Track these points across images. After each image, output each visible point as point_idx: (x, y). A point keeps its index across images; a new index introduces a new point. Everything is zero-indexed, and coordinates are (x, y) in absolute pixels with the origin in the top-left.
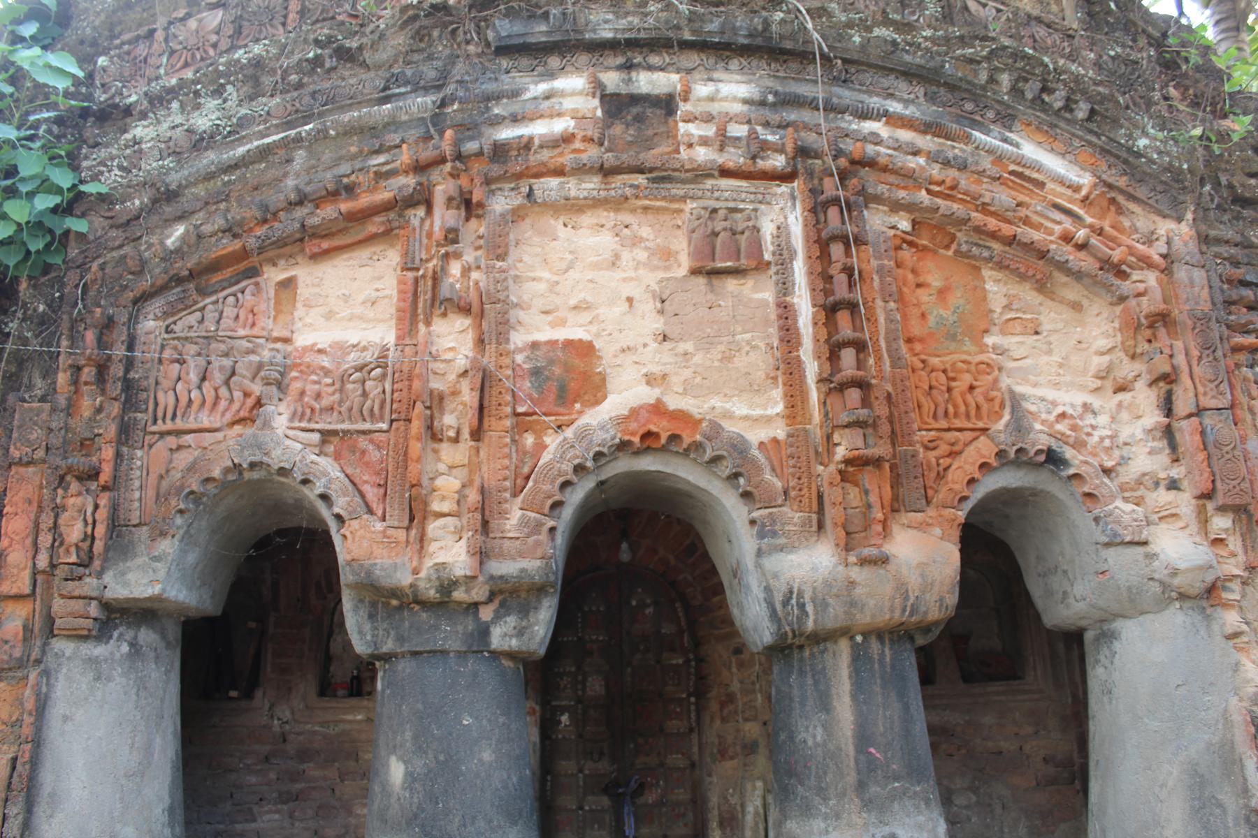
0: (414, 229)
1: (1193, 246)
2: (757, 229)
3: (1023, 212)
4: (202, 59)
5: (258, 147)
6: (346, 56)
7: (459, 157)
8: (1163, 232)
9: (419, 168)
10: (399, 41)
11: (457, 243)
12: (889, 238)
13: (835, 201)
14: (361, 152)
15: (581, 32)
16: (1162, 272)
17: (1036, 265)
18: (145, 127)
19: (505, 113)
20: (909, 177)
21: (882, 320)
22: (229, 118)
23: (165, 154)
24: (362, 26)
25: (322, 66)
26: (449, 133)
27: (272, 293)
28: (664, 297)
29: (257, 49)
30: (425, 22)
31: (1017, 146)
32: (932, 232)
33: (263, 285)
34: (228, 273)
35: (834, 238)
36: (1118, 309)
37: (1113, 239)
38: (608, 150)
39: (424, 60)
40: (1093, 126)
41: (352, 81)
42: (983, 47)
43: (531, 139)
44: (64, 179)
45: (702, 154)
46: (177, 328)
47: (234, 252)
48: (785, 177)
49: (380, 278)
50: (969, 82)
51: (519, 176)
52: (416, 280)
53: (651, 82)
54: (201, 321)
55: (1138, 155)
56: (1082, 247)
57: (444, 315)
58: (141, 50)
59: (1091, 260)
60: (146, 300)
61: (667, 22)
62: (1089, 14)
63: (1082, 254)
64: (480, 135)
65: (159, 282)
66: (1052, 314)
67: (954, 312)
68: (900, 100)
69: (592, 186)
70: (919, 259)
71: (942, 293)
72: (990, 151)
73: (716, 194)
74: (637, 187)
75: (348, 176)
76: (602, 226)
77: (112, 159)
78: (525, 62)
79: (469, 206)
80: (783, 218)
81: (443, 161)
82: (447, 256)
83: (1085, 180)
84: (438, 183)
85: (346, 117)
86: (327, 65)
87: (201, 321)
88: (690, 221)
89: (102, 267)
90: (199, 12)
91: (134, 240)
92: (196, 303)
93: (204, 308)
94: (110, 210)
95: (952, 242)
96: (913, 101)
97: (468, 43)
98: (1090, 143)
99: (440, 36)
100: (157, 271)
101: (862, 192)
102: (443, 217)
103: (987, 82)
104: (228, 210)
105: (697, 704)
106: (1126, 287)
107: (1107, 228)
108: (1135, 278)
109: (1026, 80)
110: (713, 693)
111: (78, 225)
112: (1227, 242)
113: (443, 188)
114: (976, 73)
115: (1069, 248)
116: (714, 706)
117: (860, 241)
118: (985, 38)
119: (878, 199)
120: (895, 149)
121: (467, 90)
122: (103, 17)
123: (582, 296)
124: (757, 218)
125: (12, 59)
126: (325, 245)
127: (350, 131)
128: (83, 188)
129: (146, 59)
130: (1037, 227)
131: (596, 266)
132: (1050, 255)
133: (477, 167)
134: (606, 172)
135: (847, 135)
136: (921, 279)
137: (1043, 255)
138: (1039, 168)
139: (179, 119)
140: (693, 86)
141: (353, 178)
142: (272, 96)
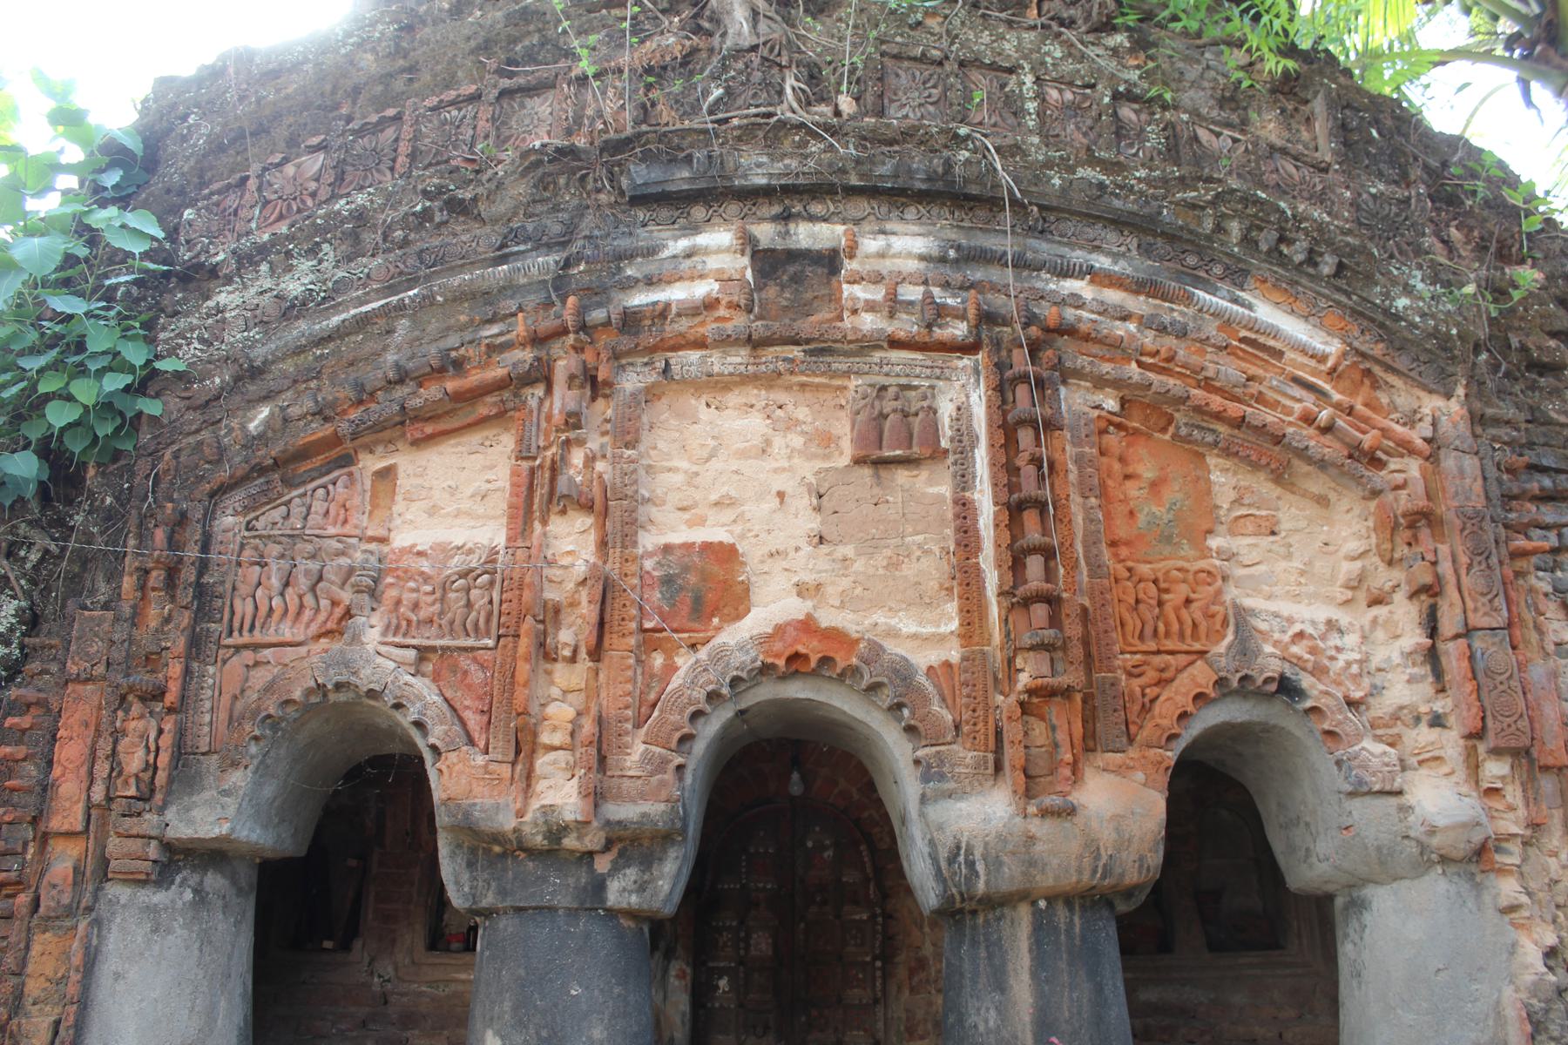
1: (1464, 428)
3: (1254, 388)
4: (299, 211)
6: (458, 208)
7: (583, 327)
9: (538, 340)
10: (520, 190)
12: (1092, 420)
13: (1024, 378)
14: (472, 321)
16: (1427, 459)
17: (1272, 454)
18: (230, 293)
19: (639, 275)
20: (1117, 349)
21: (1079, 519)
24: (477, 172)
25: (431, 220)
26: (571, 300)
29: (360, 199)
30: (549, 168)
31: (1250, 307)
32: (1144, 412)
33: (357, 475)
34: (318, 461)
35: (1021, 422)
36: (1373, 505)
37: (1366, 420)
38: (760, 317)
40: (1342, 283)
41: (464, 238)
42: (1207, 190)
43: (668, 305)
44: (136, 355)
46: (259, 525)
49: (492, 467)
50: (1191, 232)
51: (653, 350)
52: (532, 471)
53: (812, 236)
55: (1397, 317)
56: (1328, 429)
57: (563, 512)
58: (232, 201)
59: (1337, 445)
61: (830, 165)
63: (1327, 439)
65: (239, 473)
66: (1293, 510)
68: (1109, 254)
69: (739, 360)
70: (1129, 445)
71: (1155, 486)
72: (1216, 315)
73: (886, 369)
74: (792, 361)
77: (192, 330)
78: (665, 213)
79: (593, 384)
80: (963, 397)
84: (560, 358)
85: (455, 281)
86: (437, 219)
88: (854, 399)
89: (176, 456)
90: (298, 156)
91: (213, 424)
92: (281, 495)
93: (290, 501)
94: (187, 389)
95: (1170, 423)
96: (1123, 255)
97: (599, 191)
98: (1338, 303)
99: (567, 184)
101: (1058, 365)
102: (563, 399)
103: (1213, 231)
105: (883, 969)
106: (1380, 478)
107: (1359, 407)
108: (1392, 466)
109: (1261, 229)
110: (901, 957)
111: (152, 407)
112: (1508, 422)
113: (564, 364)
114: (1200, 224)
115: (1311, 431)
116: (902, 973)
117: (1052, 425)
118: (1209, 180)
119: (1078, 374)
120: (1100, 314)
121: (597, 247)
123: (724, 490)
124: (934, 396)
126: (429, 429)
127: (460, 297)
128: (158, 365)
129: (236, 213)
130: (1274, 405)
131: (743, 454)
132: (1286, 440)
133: (604, 339)
134: (756, 344)
136: (1130, 470)
137: (1278, 440)
138: (1275, 333)
140: (860, 240)
141: (462, 351)
142: (373, 255)
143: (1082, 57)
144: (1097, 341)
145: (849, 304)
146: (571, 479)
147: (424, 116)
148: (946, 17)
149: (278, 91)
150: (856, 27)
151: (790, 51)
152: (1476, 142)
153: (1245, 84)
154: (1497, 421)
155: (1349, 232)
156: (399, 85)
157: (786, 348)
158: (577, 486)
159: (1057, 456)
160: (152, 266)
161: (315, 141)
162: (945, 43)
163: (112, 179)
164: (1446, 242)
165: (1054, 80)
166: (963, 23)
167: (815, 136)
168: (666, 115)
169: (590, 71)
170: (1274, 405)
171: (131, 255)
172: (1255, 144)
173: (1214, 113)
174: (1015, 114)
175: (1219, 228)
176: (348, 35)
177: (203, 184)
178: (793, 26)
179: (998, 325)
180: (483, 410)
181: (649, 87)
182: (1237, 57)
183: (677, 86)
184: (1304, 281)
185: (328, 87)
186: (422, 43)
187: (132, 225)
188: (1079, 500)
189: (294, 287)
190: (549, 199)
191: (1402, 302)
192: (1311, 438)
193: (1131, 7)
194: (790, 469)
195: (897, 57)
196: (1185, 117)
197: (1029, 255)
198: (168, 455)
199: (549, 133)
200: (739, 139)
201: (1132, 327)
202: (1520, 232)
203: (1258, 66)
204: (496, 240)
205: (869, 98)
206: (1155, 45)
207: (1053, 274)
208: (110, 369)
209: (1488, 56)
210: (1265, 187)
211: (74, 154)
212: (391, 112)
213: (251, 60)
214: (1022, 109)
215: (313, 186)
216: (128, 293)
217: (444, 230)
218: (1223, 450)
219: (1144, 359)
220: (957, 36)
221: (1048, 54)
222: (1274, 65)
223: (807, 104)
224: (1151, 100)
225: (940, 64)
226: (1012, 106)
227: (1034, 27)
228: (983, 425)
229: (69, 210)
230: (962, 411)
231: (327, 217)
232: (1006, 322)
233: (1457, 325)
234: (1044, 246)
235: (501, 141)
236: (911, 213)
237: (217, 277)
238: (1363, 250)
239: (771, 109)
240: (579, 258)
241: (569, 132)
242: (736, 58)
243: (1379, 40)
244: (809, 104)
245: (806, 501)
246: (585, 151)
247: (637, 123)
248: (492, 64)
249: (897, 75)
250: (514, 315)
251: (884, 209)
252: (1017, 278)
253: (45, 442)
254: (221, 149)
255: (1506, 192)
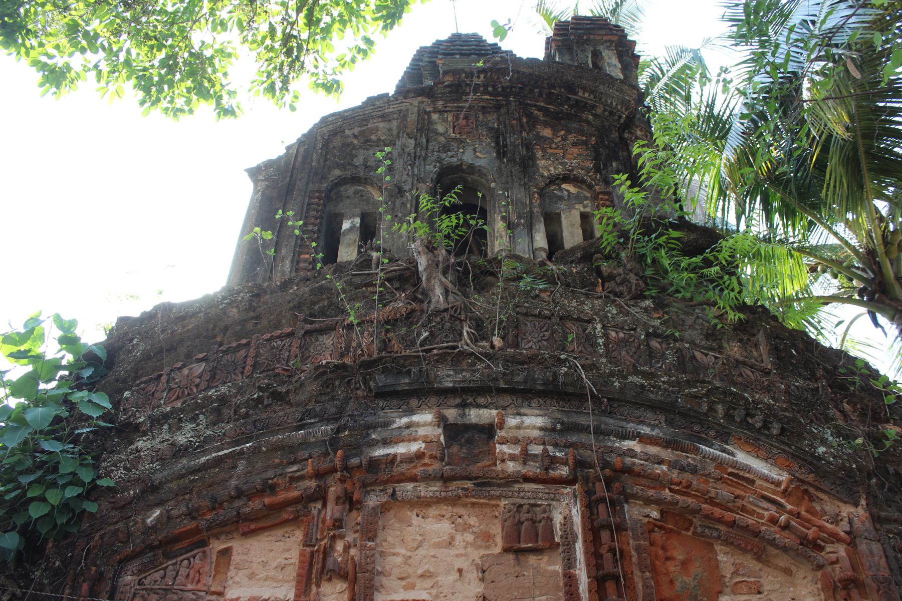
0: (313, 517)
1: (868, 524)
2: (550, 519)
3: (740, 503)
4: (189, 395)
5: (214, 458)
6: (278, 397)
7: (346, 468)
8: (845, 515)
9: (319, 475)
10: (313, 388)
11: (342, 528)
12: (644, 524)
13: (603, 500)
14: (282, 462)
15: (432, 384)
16: (849, 544)
17: (753, 543)
18: (144, 441)
19: (378, 438)
20: (657, 481)
21: (640, 586)
22: (199, 437)
23: (155, 460)
24: (290, 376)
25: (262, 403)
26: (340, 452)
27: (214, 557)
28: (485, 568)
29: (223, 389)
30: (330, 376)
31: (733, 454)
32: (675, 519)
33: (208, 553)
34: (185, 543)
35: (603, 527)
36: (819, 574)
37: (808, 521)
38: (447, 464)
39: (328, 401)
40: (785, 439)
41: (280, 414)
42: (703, 388)
43: (395, 456)
44: (86, 476)
45: (511, 467)
46: (146, 582)
47: (191, 529)
48: (568, 482)
49: (288, 550)
50: (695, 411)
51: (386, 482)
52: (312, 553)
53: (479, 416)
54: (164, 577)
55: (819, 458)
56: (786, 527)
57: (330, 580)
58: (152, 388)
59: (792, 537)
60: (128, 561)
61: (489, 376)
62: (778, 358)
63: (786, 533)
64: (361, 453)
65: (138, 549)
66: (770, 577)
67: (695, 578)
68: (648, 425)
69: (436, 489)
70: (667, 539)
71: (685, 564)
72: (714, 459)
73: (522, 494)
74: (466, 489)
75: (272, 479)
76: (443, 516)
77: (121, 462)
78: (395, 402)
79: (351, 502)
80: (568, 512)
81: (335, 471)
82: (334, 538)
83: (784, 477)
84: (331, 486)
85: (274, 439)
86: (265, 403)
87: (164, 577)
88: (503, 513)
89: (102, 537)
90: (191, 363)
91: (127, 518)
92: (161, 564)
93: (166, 567)
94: (113, 497)
95: (691, 525)
96: (657, 425)
97: (357, 389)
98: (784, 451)
99: (340, 385)
100: (138, 541)
101: (623, 492)
102: (332, 511)
103: (708, 411)
104: (190, 500)
106: (822, 557)
107: (803, 513)
108: (828, 550)
109: (735, 409)
111: (91, 507)
112: (895, 521)
113: (334, 490)
114: (700, 406)
115: (776, 528)
117: (621, 528)
118: (703, 382)
119: (635, 496)
120: (645, 460)
121: (355, 421)
122: (132, 365)
123: (427, 567)
124: (550, 511)
125: (69, 398)
126: (253, 526)
127: (275, 448)
128: (99, 482)
129: (153, 394)
130: (752, 513)
131: (438, 545)
132: (762, 534)
133: (357, 476)
134: (446, 479)
135: (612, 451)
136: (669, 554)
137: (757, 534)
138: (749, 469)
139: (167, 436)
140: (506, 419)
141: (275, 480)
142: (228, 422)
143: (628, 314)
144: (645, 477)
145: (500, 456)
146: (335, 560)
147: (262, 344)
148: (552, 292)
149: (183, 327)
150: (502, 298)
151: (466, 312)
152: (853, 353)
153: (719, 326)
154: (888, 520)
155: (786, 410)
156: (250, 326)
157: (463, 482)
158: (339, 564)
159: (624, 547)
160: (103, 424)
161: (201, 356)
162: (551, 306)
163: (87, 373)
164: (842, 412)
165: (613, 327)
166: (561, 296)
167: (480, 360)
168: (396, 346)
169: (355, 322)
170: (752, 513)
171: (92, 418)
172: (727, 360)
173: (703, 343)
174: (592, 345)
175: (711, 409)
176: (224, 298)
177: (137, 377)
178: (468, 297)
179: (587, 468)
180: (285, 516)
181: (387, 331)
182: (712, 312)
183: (403, 330)
184: (762, 438)
185: (211, 326)
186: (264, 303)
187: (94, 401)
188: (639, 574)
189: (181, 439)
190: (329, 393)
191: (821, 449)
192: (776, 533)
193: (653, 286)
194: (466, 555)
195: (526, 315)
196: (687, 345)
197: (603, 427)
198: (97, 537)
199: (331, 355)
200: (437, 361)
201: (665, 468)
202: (884, 405)
203: (725, 316)
204: (298, 416)
205: (510, 338)
206: (667, 306)
207: (617, 438)
208: (70, 483)
209: (850, 300)
210: (735, 384)
211: (69, 358)
212: (244, 341)
213: (171, 310)
214: (596, 343)
215: (198, 380)
216: (87, 438)
217: (269, 409)
218: (724, 541)
219: (673, 487)
220: (558, 303)
221: (609, 312)
222: (733, 316)
223: (475, 341)
224: (667, 336)
225: (550, 318)
226: (589, 341)
227: (601, 297)
228: (580, 528)
229: (60, 392)
230: (567, 519)
231: (204, 398)
232: (591, 466)
233: (856, 462)
234: (612, 421)
235: (304, 359)
236: (535, 403)
237: (139, 431)
238: (795, 420)
239: (455, 344)
240: (345, 427)
241: (342, 355)
242: (436, 315)
243: (790, 291)
244: (476, 341)
245: (475, 574)
246: (351, 366)
247: (380, 350)
248: (301, 316)
249: (526, 325)
250: (307, 460)
251: (519, 401)
252: (597, 440)
253: (26, 525)
254: (149, 358)
255: (872, 382)
